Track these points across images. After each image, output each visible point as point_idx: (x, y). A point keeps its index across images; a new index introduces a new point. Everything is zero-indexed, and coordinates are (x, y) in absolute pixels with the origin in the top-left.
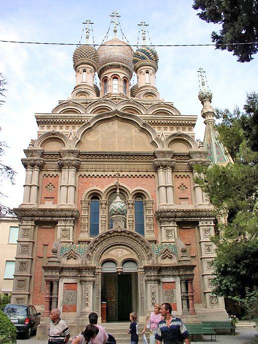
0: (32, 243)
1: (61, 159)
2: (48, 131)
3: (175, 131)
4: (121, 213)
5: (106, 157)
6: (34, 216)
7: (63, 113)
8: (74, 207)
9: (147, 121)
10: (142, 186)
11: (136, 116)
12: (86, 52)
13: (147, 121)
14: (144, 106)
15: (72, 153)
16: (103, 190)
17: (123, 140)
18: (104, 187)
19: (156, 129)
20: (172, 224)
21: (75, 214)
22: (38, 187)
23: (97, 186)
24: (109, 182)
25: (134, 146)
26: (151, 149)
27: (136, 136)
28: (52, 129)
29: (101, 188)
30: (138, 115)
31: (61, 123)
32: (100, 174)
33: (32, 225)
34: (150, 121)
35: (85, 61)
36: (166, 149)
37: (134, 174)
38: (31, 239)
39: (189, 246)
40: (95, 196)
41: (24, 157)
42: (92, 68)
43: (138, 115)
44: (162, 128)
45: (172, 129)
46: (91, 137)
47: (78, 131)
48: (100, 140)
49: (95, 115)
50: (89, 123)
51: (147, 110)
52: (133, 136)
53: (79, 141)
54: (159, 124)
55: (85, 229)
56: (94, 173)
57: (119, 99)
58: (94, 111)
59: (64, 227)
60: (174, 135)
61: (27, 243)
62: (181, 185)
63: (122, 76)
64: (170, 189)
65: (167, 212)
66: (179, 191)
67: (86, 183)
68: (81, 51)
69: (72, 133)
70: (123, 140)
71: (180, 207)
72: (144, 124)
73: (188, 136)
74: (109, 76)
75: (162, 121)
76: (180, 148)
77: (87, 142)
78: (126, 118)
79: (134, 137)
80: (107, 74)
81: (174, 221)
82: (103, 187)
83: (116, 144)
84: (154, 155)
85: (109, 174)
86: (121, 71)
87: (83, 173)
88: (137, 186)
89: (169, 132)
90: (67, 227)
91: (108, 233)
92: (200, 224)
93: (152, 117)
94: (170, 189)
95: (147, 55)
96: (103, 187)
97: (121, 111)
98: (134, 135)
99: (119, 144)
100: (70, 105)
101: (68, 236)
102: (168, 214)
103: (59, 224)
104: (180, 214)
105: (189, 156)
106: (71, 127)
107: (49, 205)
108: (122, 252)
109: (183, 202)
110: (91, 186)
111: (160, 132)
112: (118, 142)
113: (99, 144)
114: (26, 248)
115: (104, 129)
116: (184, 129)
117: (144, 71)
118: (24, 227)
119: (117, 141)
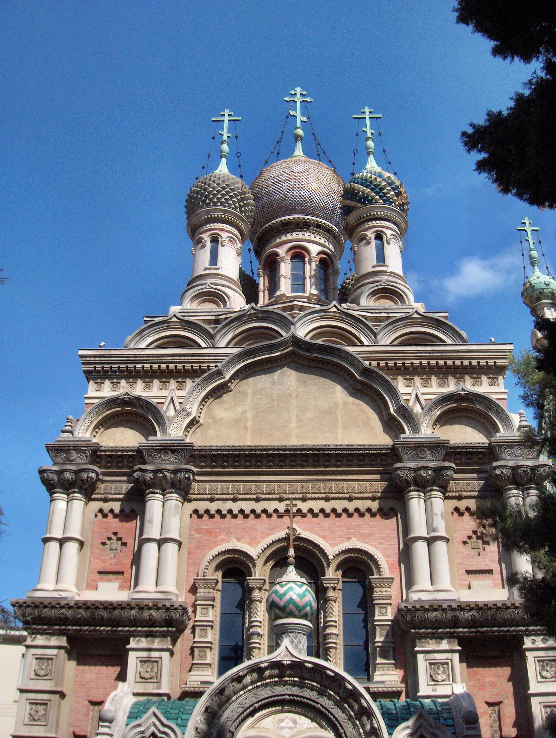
0: (58, 696)
1: (143, 467)
2: (445, 390)
3: (451, 387)
4: (297, 612)
5: (378, 461)
6: (64, 621)
7: (160, 347)
8: (182, 597)
9: (374, 363)
10: (363, 537)
11: (347, 353)
12: (218, 191)
13: (374, 363)
14: (370, 324)
15: (173, 451)
16: (253, 552)
17: (310, 415)
18: (257, 544)
19: (401, 385)
20: (444, 645)
21: (176, 615)
22: (82, 544)
23: (239, 540)
24: (272, 530)
25: (340, 430)
26: (382, 439)
27: (345, 403)
28: (123, 389)
29: (250, 544)
30: (350, 349)
31: (148, 376)
32: (247, 506)
33: (60, 648)
34: (382, 363)
35: (217, 215)
36: (427, 431)
37: (339, 505)
38: (56, 685)
39: (496, 708)
40: (235, 567)
41: (48, 463)
42: (236, 232)
43: (350, 349)
44: (418, 381)
45: (443, 382)
46: (226, 409)
47: (190, 394)
48: (249, 415)
49: (235, 351)
50: (219, 373)
51: (375, 335)
52: (336, 404)
53: (194, 419)
54: (409, 372)
55: (203, 657)
56: (230, 505)
57: (301, 308)
58: (238, 341)
59: (144, 654)
60: (113, 402)
61: (45, 696)
62: (470, 533)
63: (314, 249)
64: (171, 549)
65: (433, 609)
66: (466, 550)
67: (209, 532)
68: (205, 190)
69: (175, 399)
70: (310, 415)
71: (466, 596)
72: (366, 372)
73: (487, 399)
74: (281, 251)
75: (416, 362)
76: (126, 438)
77: (215, 420)
78: (319, 359)
79: (341, 406)
80: (277, 246)
81: (451, 636)
82: (256, 541)
83: (293, 425)
84: (392, 455)
85: (271, 506)
86: (312, 237)
87: (202, 506)
88: (349, 539)
89: (435, 389)
90: (154, 654)
91: (307, 728)
92: (528, 643)
93: (388, 352)
94: (72, 548)
95: (377, 193)
96: (256, 541)
97: (308, 338)
98: (340, 401)
99: (298, 427)
100: (174, 328)
101: (157, 679)
102: (432, 615)
103: (133, 644)
104: (467, 615)
105: (490, 453)
106: (173, 384)
107: (110, 592)
108: (295, 722)
109: (477, 581)
110: (222, 540)
111: (409, 390)
112: (299, 420)
113: (246, 428)
114: (41, 708)
115: (260, 386)
116: (477, 381)
117: (370, 234)
118: (40, 651)
119: (294, 418)
